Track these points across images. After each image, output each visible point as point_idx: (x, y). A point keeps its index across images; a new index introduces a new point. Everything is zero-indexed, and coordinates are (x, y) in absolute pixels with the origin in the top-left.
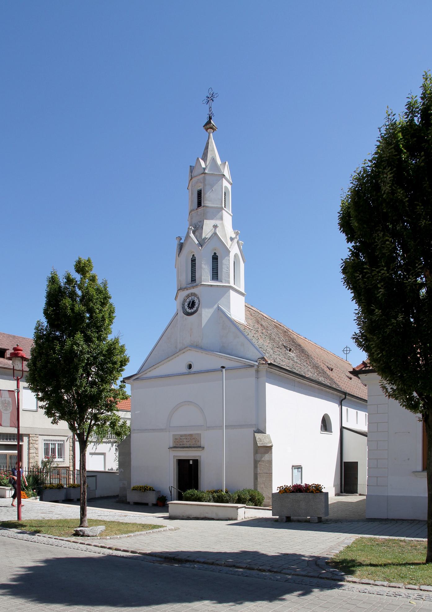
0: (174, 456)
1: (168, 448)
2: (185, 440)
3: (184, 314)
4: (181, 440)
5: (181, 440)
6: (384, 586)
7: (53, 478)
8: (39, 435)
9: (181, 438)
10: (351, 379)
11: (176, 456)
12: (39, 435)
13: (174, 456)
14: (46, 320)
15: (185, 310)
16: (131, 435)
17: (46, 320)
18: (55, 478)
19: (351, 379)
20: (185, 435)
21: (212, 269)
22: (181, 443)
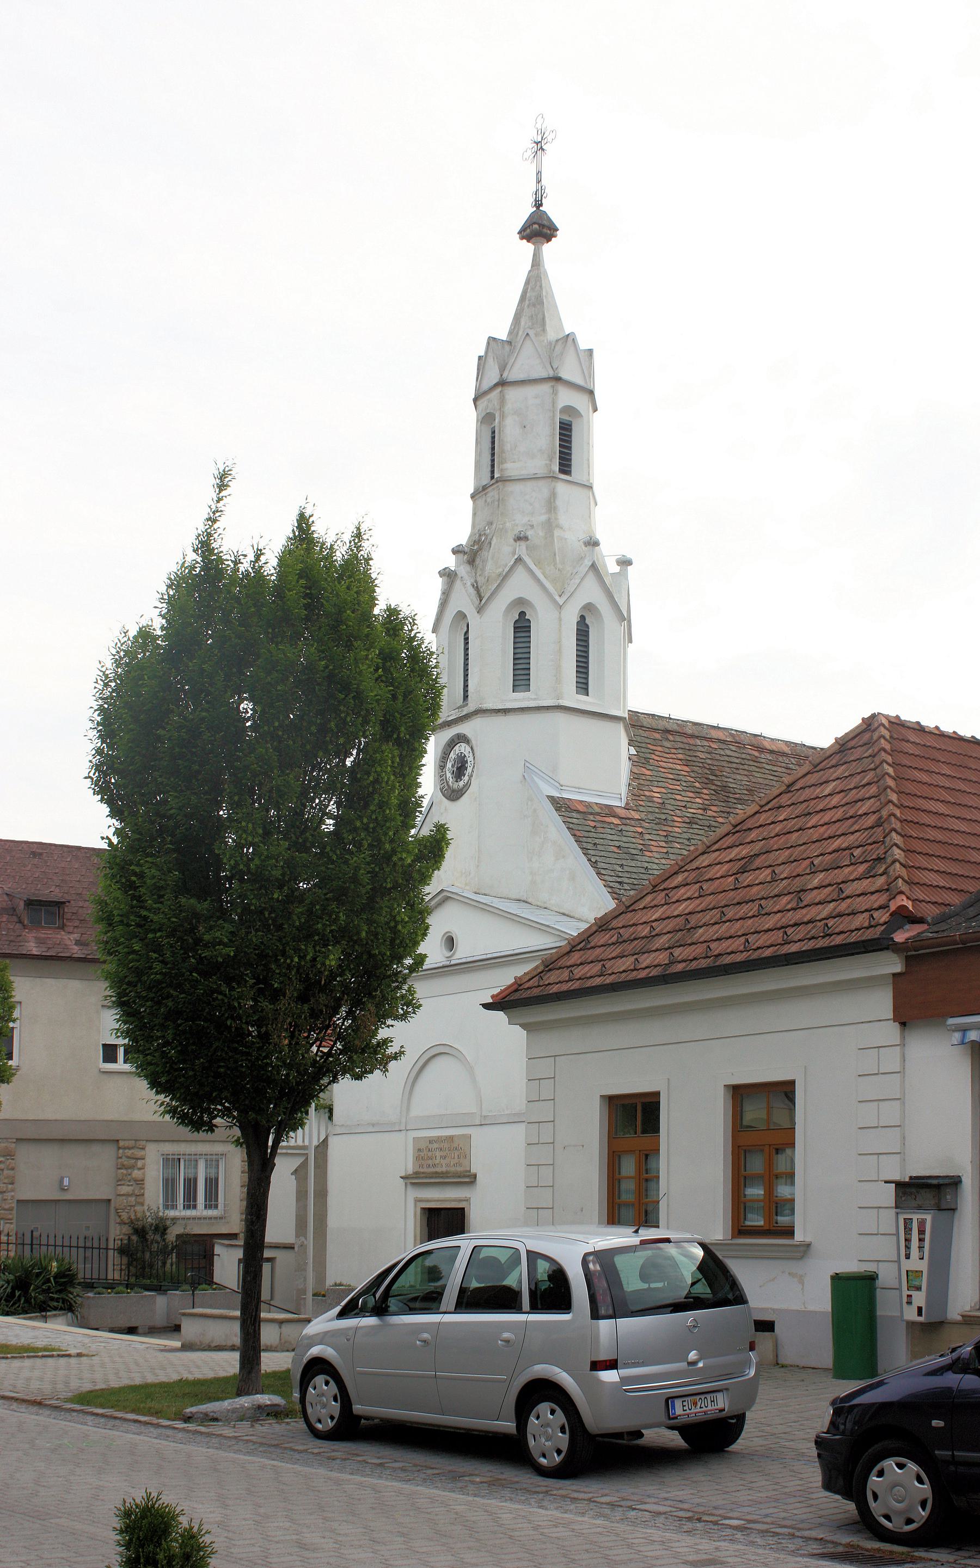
0: (417, 1201)
1: (401, 1177)
2: (438, 1154)
3: (444, 795)
4: (430, 1154)
5: (430, 1154)
6: (539, 173)
7: (55, 1246)
8: (147, 1141)
9: (430, 1146)
10: (954, 1350)
11: (421, 1201)
12: (147, 1141)
13: (417, 1201)
14: (115, 840)
15: (445, 784)
16: (333, 1141)
17: (115, 840)
18: (99, 1248)
19: (954, 1350)
20: (439, 1140)
21: (514, 659)
22: (430, 1162)
